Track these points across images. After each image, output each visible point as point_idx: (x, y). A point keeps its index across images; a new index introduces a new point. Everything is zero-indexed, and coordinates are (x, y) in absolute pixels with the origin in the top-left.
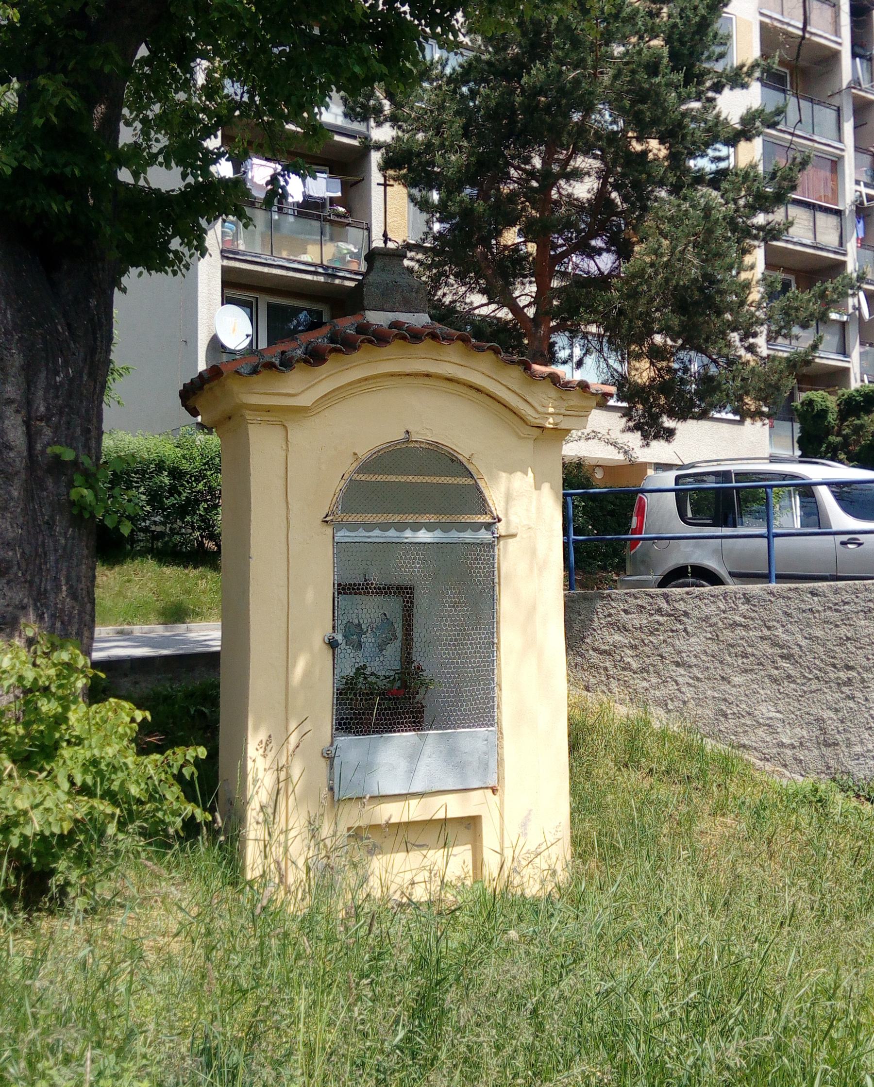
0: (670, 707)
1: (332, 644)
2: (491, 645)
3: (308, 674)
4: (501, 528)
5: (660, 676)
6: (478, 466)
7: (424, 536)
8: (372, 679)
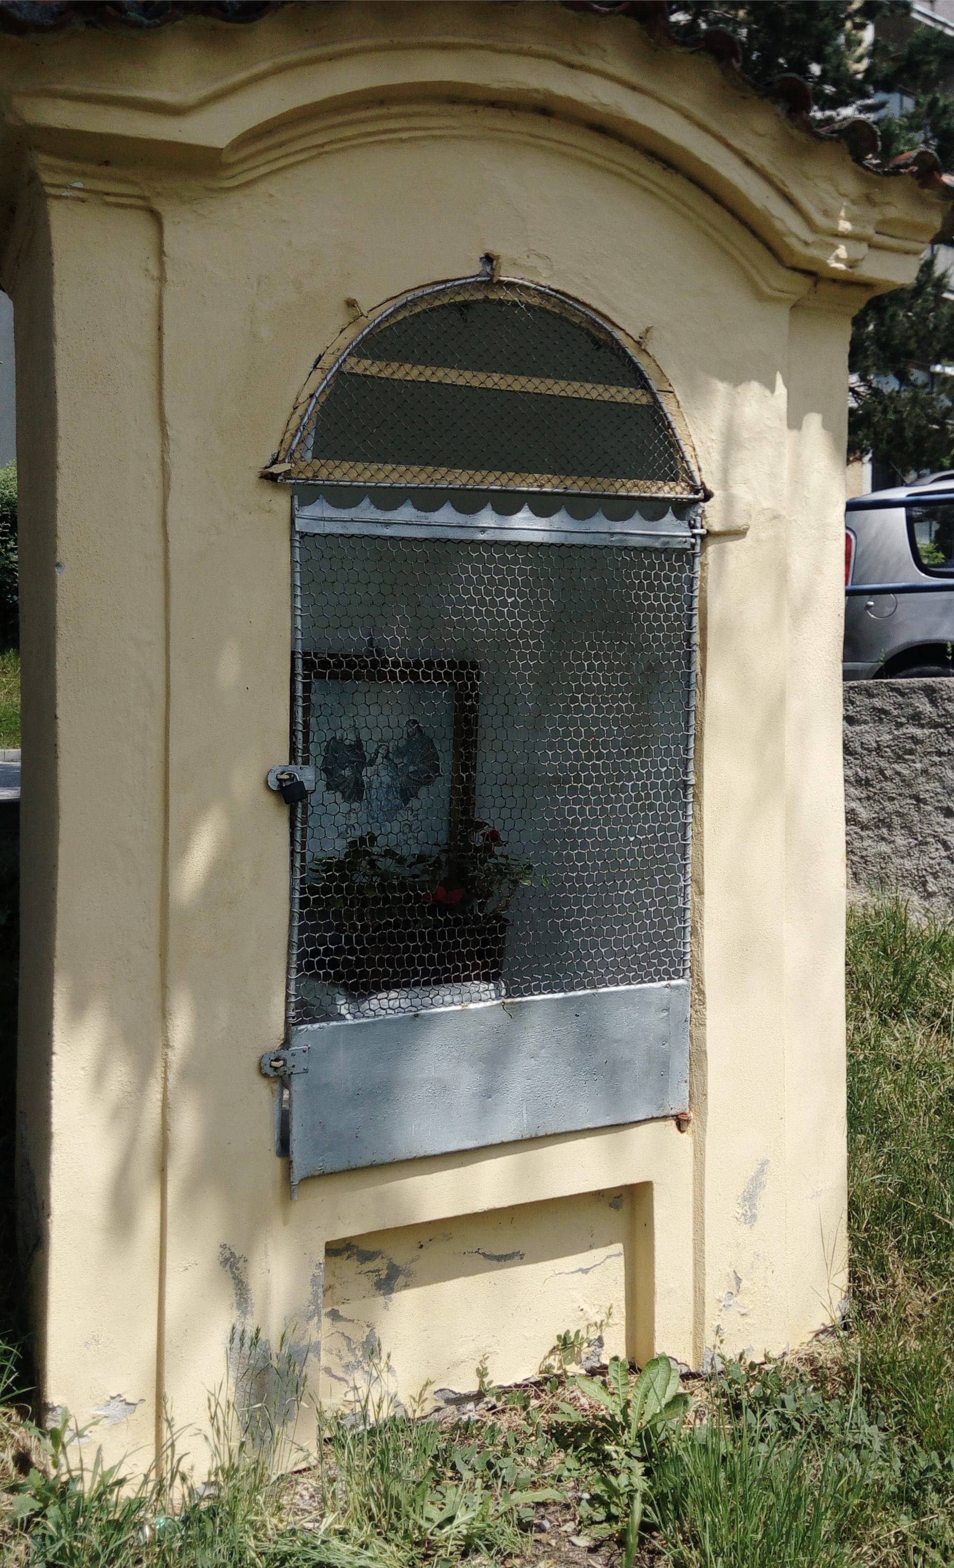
0: (931, 887)
1: (289, 793)
2: (682, 790)
3: (221, 868)
4: (713, 515)
5: (912, 834)
6: (665, 361)
7: (526, 526)
8: (385, 864)
